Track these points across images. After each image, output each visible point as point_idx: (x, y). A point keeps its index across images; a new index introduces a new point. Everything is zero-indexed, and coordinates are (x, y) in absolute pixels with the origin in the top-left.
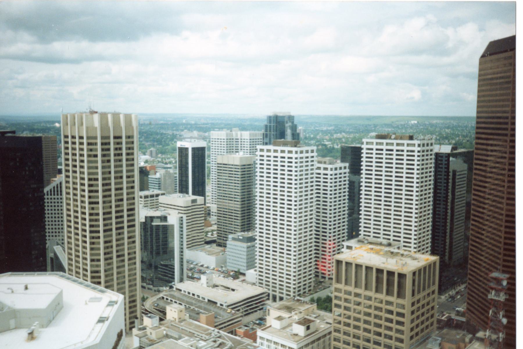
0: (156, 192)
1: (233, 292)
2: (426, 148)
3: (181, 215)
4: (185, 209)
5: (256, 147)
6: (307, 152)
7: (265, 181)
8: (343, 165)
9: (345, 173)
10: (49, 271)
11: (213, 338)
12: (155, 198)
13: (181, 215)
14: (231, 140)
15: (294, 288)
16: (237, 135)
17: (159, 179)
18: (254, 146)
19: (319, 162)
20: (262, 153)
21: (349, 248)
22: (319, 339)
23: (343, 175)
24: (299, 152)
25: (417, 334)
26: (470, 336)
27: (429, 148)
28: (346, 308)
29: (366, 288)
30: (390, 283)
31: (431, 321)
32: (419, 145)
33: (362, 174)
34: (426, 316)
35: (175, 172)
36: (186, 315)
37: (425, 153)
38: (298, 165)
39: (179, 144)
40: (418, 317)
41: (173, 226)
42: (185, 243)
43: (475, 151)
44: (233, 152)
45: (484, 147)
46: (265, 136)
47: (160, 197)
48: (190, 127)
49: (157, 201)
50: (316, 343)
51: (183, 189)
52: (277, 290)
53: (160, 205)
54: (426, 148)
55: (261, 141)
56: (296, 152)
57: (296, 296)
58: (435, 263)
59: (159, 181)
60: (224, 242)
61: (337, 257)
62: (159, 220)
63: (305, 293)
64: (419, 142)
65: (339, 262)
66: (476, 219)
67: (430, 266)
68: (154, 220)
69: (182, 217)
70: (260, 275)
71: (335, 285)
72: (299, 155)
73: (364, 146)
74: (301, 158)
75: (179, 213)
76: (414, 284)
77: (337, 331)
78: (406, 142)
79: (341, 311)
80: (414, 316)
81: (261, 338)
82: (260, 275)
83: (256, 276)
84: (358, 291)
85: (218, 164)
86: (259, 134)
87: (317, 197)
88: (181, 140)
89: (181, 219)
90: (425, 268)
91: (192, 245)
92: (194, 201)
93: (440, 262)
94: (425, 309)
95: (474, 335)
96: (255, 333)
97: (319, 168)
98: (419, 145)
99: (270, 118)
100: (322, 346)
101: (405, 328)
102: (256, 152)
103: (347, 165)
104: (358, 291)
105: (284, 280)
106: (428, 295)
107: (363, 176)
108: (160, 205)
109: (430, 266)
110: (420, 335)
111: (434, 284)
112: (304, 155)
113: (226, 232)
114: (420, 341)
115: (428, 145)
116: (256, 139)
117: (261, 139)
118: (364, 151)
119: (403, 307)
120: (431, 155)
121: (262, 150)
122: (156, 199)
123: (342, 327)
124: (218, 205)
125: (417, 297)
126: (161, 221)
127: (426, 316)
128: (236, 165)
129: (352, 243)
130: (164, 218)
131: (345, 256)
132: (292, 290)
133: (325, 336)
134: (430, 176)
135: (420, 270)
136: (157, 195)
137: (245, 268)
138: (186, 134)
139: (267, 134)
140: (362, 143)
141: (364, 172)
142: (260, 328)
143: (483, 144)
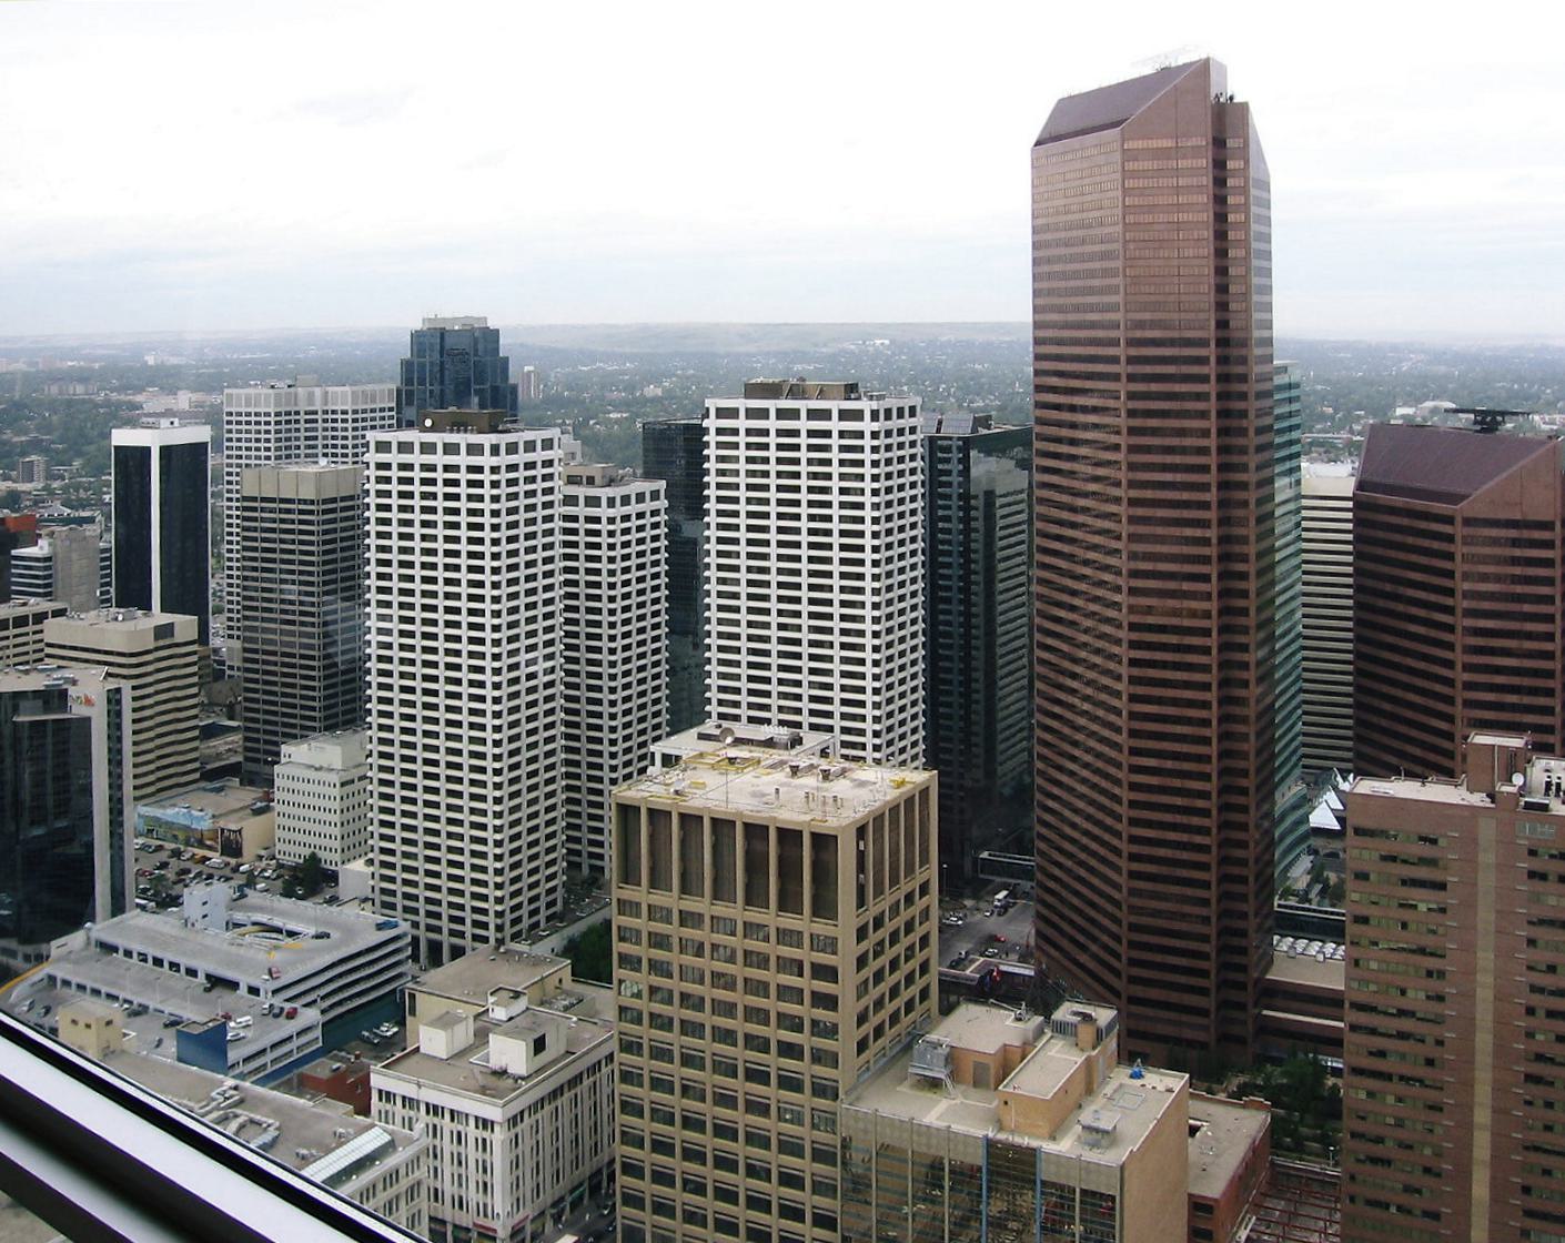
0: (37, 605)
1: (290, 940)
2: (895, 424)
3: (113, 684)
4: (134, 661)
5: (364, 437)
6: (530, 446)
7: (805, 712)
8: (647, 486)
9: (654, 513)
10: (844, 828)
11: (217, 1108)
12: (31, 628)
13: (113, 684)
14: (293, 417)
15: (499, 914)
16: (311, 397)
17: (48, 559)
18: (360, 433)
19: (572, 480)
20: (384, 458)
21: (670, 761)
22: (575, 1081)
23: (648, 521)
24: (503, 450)
25: (879, 1032)
26: (1039, 1019)
27: (907, 422)
28: (657, 967)
29: (717, 895)
30: (789, 870)
31: (920, 983)
32: (875, 416)
33: (707, 512)
34: (905, 968)
35: (102, 535)
36: (125, 1035)
37: (895, 440)
38: (503, 491)
39: (123, 437)
40: (879, 977)
41: (85, 722)
42: (128, 783)
43: (1037, 429)
44: (298, 456)
45: (1065, 498)
46: (404, 397)
47: (49, 622)
48: (167, 379)
49: (38, 637)
50: (548, 1108)
51: (132, 595)
52: (445, 924)
53: (49, 650)
54: (895, 424)
55: (391, 418)
56: (495, 450)
57: (508, 939)
58: (925, 792)
59: (46, 568)
60: (267, 769)
61: (629, 794)
62: (39, 703)
63: (536, 925)
64: (874, 405)
65: (627, 812)
66: (1050, 641)
67: (911, 803)
68: (23, 704)
69: (118, 690)
70: (384, 878)
71: (618, 892)
72: (504, 460)
73: (712, 423)
74: (512, 468)
75: (109, 675)
76: (861, 868)
77: (630, 1046)
78: (834, 406)
79: (642, 979)
80: (868, 972)
81: (387, 1096)
82: (384, 878)
83: (372, 883)
84: (691, 904)
85: (245, 499)
86: (385, 390)
87: (569, 596)
88: (132, 423)
89: (114, 698)
90: (894, 810)
91: (161, 786)
92: (164, 631)
93: (941, 785)
94: (900, 948)
95: (1048, 1017)
96: (365, 1082)
97: (570, 500)
98: (875, 416)
99: (417, 336)
100: (588, 1103)
101: (845, 1016)
102: (363, 454)
103: (662, 485)
104: (691, 904)
105: (443, 882)
106: (909, 899)
107: (712, 519)
108: (49, 650)
109: (909, 801)
110: (890, 1033)
111: (925, 860)
112: (520, 458)
113: (275, 733)
114: (890, 1054)
115: (900, 414)
116: (373, 411)
117: (391, 409)
118: (711, 438)
119: (830, 945)
120: (913, 444)
121: (383, 447)
122: (35, 633)
123: (646, 1033)
124: (246, 640)
125: (873, 910)
126: (47, 709)
127: (905, 968)
128: (305, 502)
129: (684, 743)
130: (55, 697)
131: (651, 790)
132: (491, 920)
133: (595, 1068)
134: (913, 512)
135: (879, 819)
136: (40, 618)
137: (337, 857)
138: (151, 401)
139: (410, 394)
140: (706, 415)
141: (712, 506)
142: (379, 1058)
143: (1057, 407)
